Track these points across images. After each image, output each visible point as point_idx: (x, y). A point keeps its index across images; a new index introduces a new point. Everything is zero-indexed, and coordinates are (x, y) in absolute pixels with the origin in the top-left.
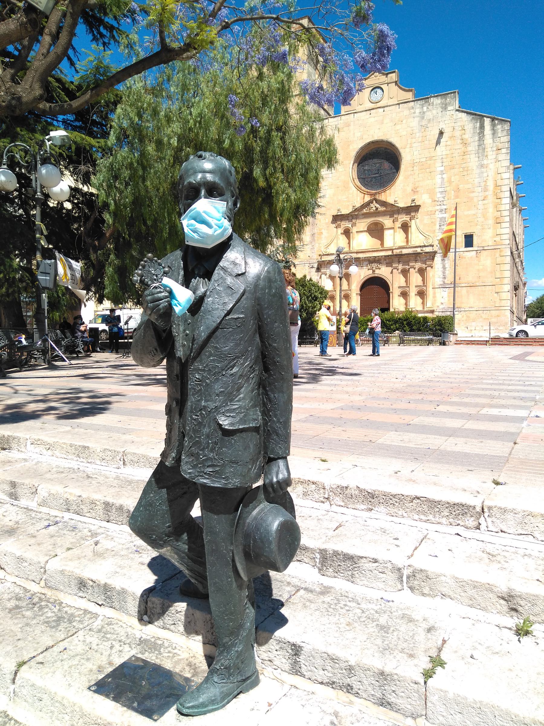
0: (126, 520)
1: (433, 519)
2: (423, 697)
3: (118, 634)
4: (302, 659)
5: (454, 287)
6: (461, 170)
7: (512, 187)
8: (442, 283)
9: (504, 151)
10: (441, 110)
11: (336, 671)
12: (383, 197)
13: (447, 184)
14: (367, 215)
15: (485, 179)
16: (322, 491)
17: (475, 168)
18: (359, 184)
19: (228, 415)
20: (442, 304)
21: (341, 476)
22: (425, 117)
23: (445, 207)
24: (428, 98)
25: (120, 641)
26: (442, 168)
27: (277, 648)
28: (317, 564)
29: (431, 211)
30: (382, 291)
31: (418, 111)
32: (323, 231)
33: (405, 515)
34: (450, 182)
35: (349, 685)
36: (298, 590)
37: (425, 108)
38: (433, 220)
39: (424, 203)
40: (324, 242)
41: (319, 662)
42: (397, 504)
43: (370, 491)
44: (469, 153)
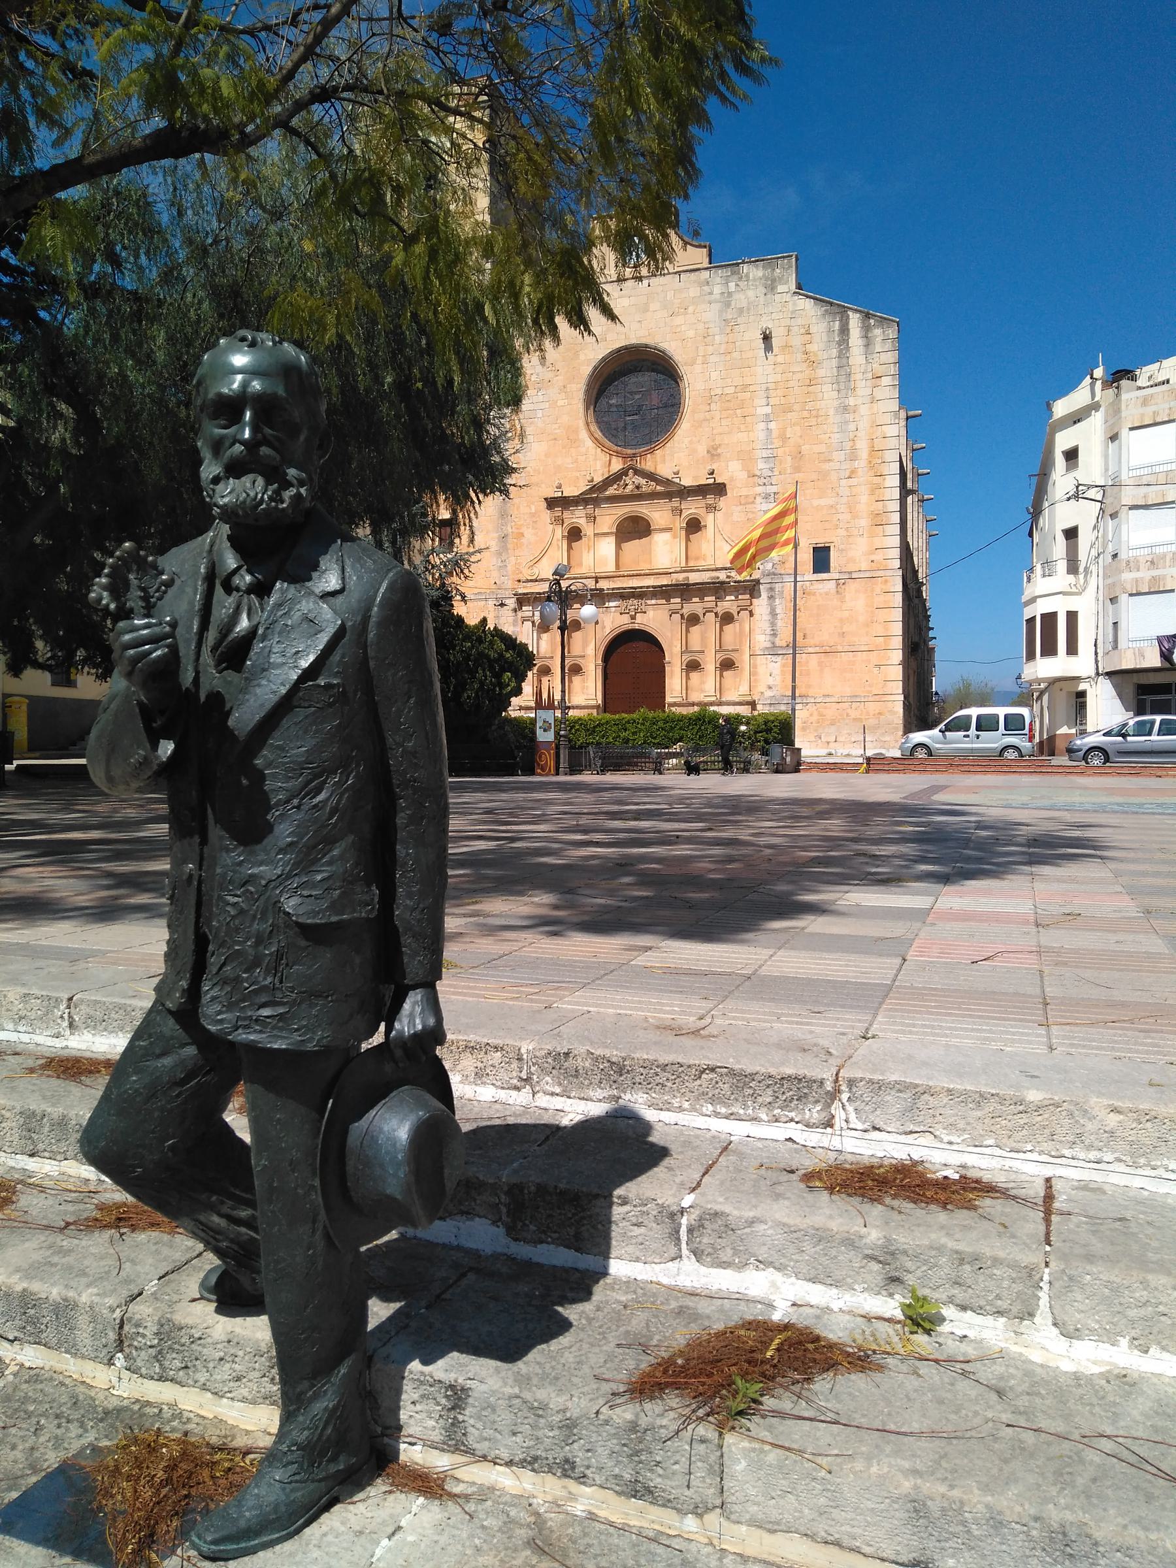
0: (75, 1148)
1: (741, 1112)
2: (717, 1468)
3: (54, 1401)
4: (468, 1415)
5: (794, 654)
6: (806, 414)
7: (904, 454)
8: (769, 645)
9: (886, 381)
10: (764, 291)
11: (540, 1434)
12: (648, 464)
13: (777, 443)
14: (614, 499)
15: (852, 435)
16: (515, 1065)
17: (831, 412)
18: (598, 434)
19: (305, 893)
20: (770, 688)
21: (555, 1032)
22: (733, 303)
23: (774, 489)
24: (738, 264)
25: (57, 1416)
26: (768, 410)
27: (416, 1397)
28: (504, 1218)
29: (747, 496)
30: (642, 645)
31: (717, 290)
32: (524, 530)
33: (686, 1105)
34: (784, 438)
35: (567, 1461)
36: (464, 1275)
37: (732, 285)
38: (751, 516)
39: (732, 479)
40: (526, 555)
41: (504, 1418)
42: (669, 1084)
43: (614, 1060)
44: (820, 381)
